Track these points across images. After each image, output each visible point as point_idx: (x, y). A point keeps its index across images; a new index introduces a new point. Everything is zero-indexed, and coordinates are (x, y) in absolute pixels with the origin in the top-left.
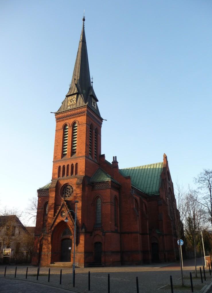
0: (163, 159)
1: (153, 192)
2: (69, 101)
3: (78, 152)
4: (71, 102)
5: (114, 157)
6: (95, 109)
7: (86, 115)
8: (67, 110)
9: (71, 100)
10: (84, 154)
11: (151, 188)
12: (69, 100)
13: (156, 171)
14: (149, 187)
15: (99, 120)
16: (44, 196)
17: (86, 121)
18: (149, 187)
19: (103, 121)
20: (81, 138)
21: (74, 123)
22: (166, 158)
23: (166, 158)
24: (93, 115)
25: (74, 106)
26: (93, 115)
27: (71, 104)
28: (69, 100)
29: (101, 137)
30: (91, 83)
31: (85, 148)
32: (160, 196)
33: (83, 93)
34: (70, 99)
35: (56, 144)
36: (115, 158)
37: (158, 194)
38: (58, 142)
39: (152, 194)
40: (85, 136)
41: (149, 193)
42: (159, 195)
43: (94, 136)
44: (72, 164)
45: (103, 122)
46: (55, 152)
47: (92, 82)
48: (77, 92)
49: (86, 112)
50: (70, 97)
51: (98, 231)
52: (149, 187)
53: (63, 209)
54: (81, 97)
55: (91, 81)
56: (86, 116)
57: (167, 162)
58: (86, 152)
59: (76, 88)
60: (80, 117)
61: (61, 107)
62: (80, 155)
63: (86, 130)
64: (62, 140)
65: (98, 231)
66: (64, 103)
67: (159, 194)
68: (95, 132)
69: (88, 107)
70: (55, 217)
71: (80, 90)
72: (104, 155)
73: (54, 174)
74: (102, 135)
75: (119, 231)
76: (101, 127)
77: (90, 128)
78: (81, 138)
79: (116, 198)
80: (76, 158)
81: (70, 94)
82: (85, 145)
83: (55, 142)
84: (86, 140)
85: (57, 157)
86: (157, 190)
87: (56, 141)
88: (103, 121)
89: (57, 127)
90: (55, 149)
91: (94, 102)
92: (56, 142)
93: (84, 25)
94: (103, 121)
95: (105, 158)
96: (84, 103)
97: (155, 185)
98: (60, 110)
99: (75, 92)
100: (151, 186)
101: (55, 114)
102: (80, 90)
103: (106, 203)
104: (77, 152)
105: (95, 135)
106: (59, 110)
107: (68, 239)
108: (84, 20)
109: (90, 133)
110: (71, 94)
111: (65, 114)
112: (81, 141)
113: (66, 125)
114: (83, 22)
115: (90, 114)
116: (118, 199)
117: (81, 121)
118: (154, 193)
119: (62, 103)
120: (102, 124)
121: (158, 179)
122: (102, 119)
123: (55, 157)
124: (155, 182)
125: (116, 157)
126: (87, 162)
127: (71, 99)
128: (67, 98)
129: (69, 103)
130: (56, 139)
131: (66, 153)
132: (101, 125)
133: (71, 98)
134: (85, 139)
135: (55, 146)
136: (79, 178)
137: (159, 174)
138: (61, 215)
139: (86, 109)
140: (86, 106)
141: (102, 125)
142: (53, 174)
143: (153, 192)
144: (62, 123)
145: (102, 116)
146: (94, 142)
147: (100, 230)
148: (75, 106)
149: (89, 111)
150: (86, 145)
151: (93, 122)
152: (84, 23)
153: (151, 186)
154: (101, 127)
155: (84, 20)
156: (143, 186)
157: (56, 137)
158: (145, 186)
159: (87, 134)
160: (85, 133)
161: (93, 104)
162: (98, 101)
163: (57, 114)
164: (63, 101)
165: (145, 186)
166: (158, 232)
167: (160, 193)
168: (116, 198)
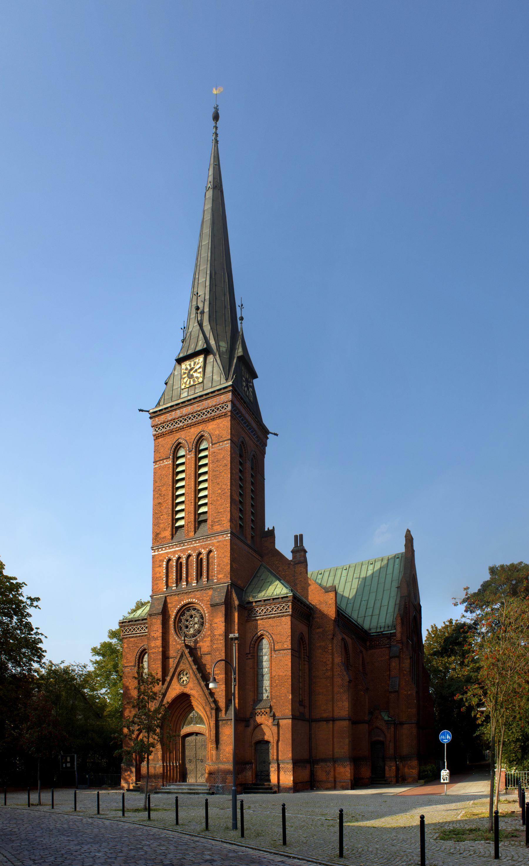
0: (405, 546)
1: (379, 626)
2: (184, 376)
3: (212, 521)
4: (190, 377)
5: (296, 537)
6: (250, 400)
7: (229, 414)
8: (180, 401)
9: (189, 372)
10: (227, 525)
11: (375, 618)
12: (185, 373)
13: (387, 576)
14: (372, 616)
15: (259, 433)
16: (136, 637)
17: (231, 434)
18: (370, 614)
19: (268, 436)
20: (218, 480)
21: (200, 439)
22: (409, 540)
23: (409, 540)
24: (247, 416)
25: (199, 392)
26: (247, 416)
27: (190, 383)
28: (185, 373)
29: (265, 481)
30: (239, 322)
31: (229, 509)
32: (395, 636)
33: (221, 349)
34: (186, 369)
35: (157, 501)
36: (299, 539)
37: (392, 632)
38: (160, 495)
39: (378, 630)
40: (229, 476)
41: (370, 629)
42: (395, 632)
43: (249, 487)
44: (200, 554)
45: (268, 441)
46: (156, 524)
47: (242, 319)
48: (205, 346)
49: (229, 405)
50: (187, 363)
51: (263, 716)
52: (372, 616)
53: (181, 667)
54: (215, 363)
55: (239, 316)
56: (229, 418)
57: (413, 551)
58: (231, 520)
59: (201, 335)
60: (215, 422)
61: (164, 394)
62: (217, 528)
63: (231, 457)
64: (170, 488)
65: (263, 716)
66: (170, 382)
67: (394, 631)
68: (252, 469)
69: (235, 390)
70: (166, 684)
71: (212, 342)
72: (271, 533)
73: (155, 580)
74: (266, 477)
75: (307, 716)
76: (265, 454)
77: (241, 456)
78: (218, 480)
79: (302, 640)
80: (208, 537)
81: (185, 354)
82: (229, 500)
83: (154, 495)
84: (231, 486)
85: (160, 536)
86: (389, 621)
87: (157, 506)
88: (269, 436)
89: (156, 451)
90: (155, 514)
91: (246, 379)
92: (157, 496)
93: (217, 135)
94: (268, 436)
95: (274, 543)
96: (223, 380)
97: (384, 609)
98: (162, 400)
99: (199, 348)
100: (377, 612)
101: (149, 416)
102: (212, 342)
103: (281, 652)
104: (209, 522)
105: (252, 498)
106: (159, 404)
107: (197, 735)
108: (216, 117)
109: (240, 507)
110: (190, 352)
111: (178, 413)
112: (220, 491)
113: (178, 446)
114: (213, 123)
115: (240, 412)
116: (307, 642)
117: (217, 432)
118: (382, 630)
119: (166, 384)
120: (266, 446)
121: (401, 571)
122: (266, 432)
123: (156, 536)
124: (385, 603)
125: (301, 536)
126: (235, 547)
127: (189, 368)
128: (178, 367)
129: (185, 380)
130: (157, 484)
131: (181, 523)
132: (265, 449)
133: (190, 365)
134: (229, 484)
135: (155, 505)
136: (217, 588)
137: (395, 584)
138: (179, 679)
139: (229, 396)
140: (231, 388)
141: (266, 448)
142: (153, 578)
143: (379, 626)
144: (169, 442)
145: (267, 421)
146: (249, 502)
147: (267, 713)
148: (201, 389)
149: (238, 404)
150: (232, 501)
151: (247, 439)
152: (216, 128)
153: (377, 612)
154: (263, 453)
155: (216, 117)
156: (357, 612)
157: (155, 482)
158: (362, 614)
159: (234, 472)
160: (229, 466)
161: (244, 384)
162: (255, 376)
163: (154, 415)
164: (169, 378)
165: (362, 614)
166: (386, 718)
167: (395, 629)
168: (301, 638)
